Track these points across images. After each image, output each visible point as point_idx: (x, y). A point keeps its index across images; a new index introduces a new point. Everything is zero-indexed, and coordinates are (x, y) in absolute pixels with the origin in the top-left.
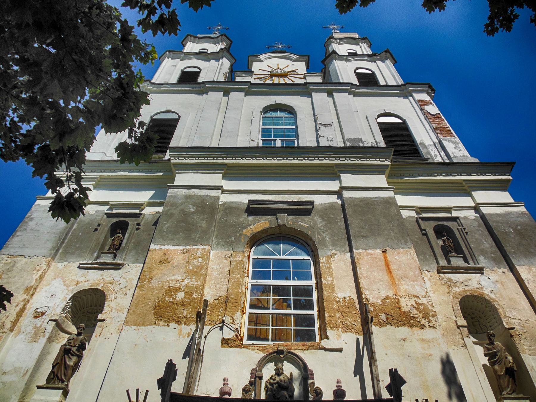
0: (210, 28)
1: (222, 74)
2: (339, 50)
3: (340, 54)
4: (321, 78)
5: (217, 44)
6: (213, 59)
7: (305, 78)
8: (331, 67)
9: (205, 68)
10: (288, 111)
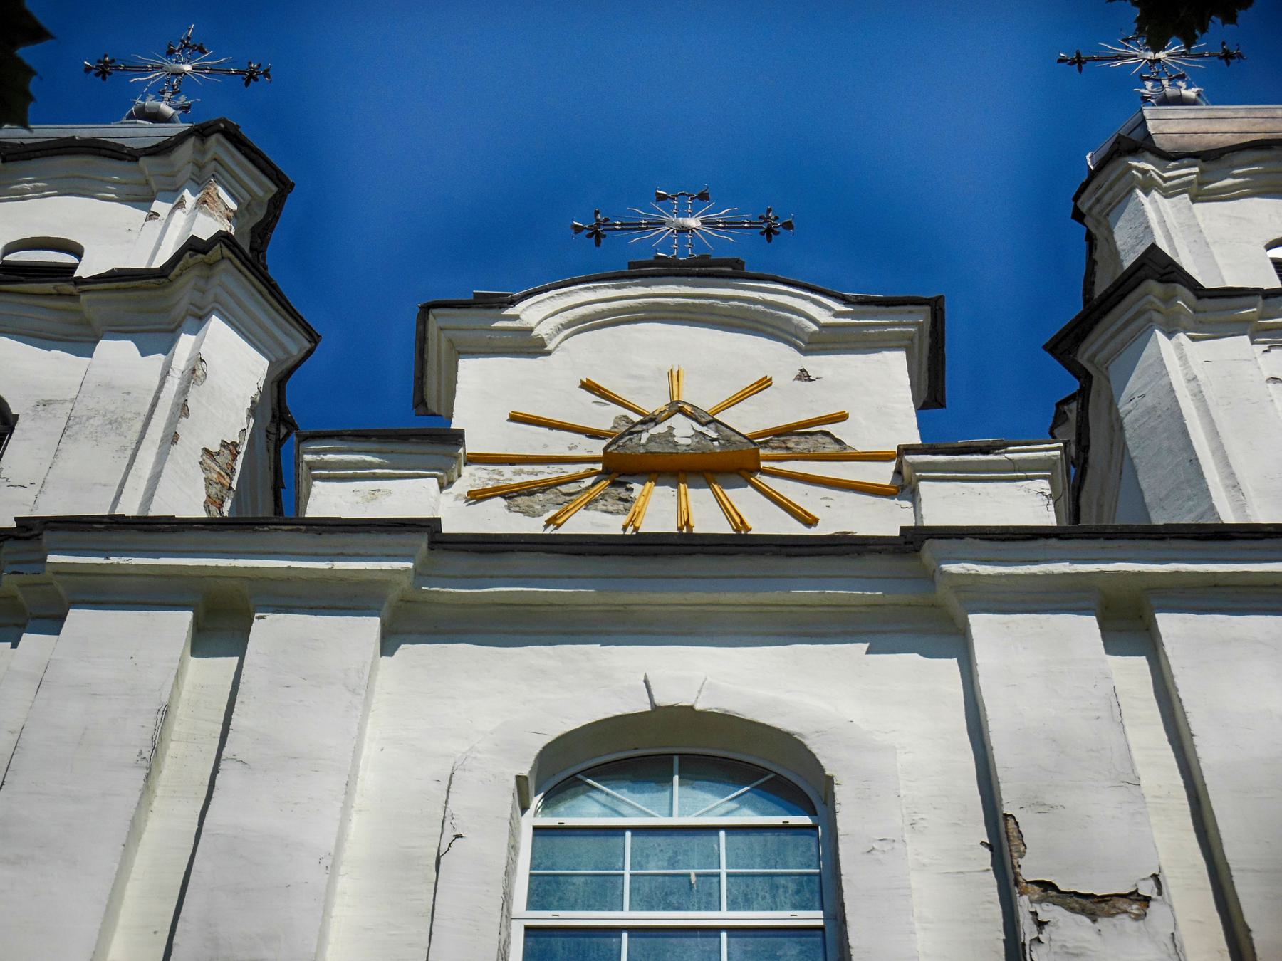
0: (103, 72)
1: (186, 456)
2: (1202, 245)
3: (1208, 282)
4: (1044, 485)
5: (157, 206)
6: (118, 332)
7: (904, 488)
8: (1133, 385)
9: (46, 403)
10: (763, 771)
